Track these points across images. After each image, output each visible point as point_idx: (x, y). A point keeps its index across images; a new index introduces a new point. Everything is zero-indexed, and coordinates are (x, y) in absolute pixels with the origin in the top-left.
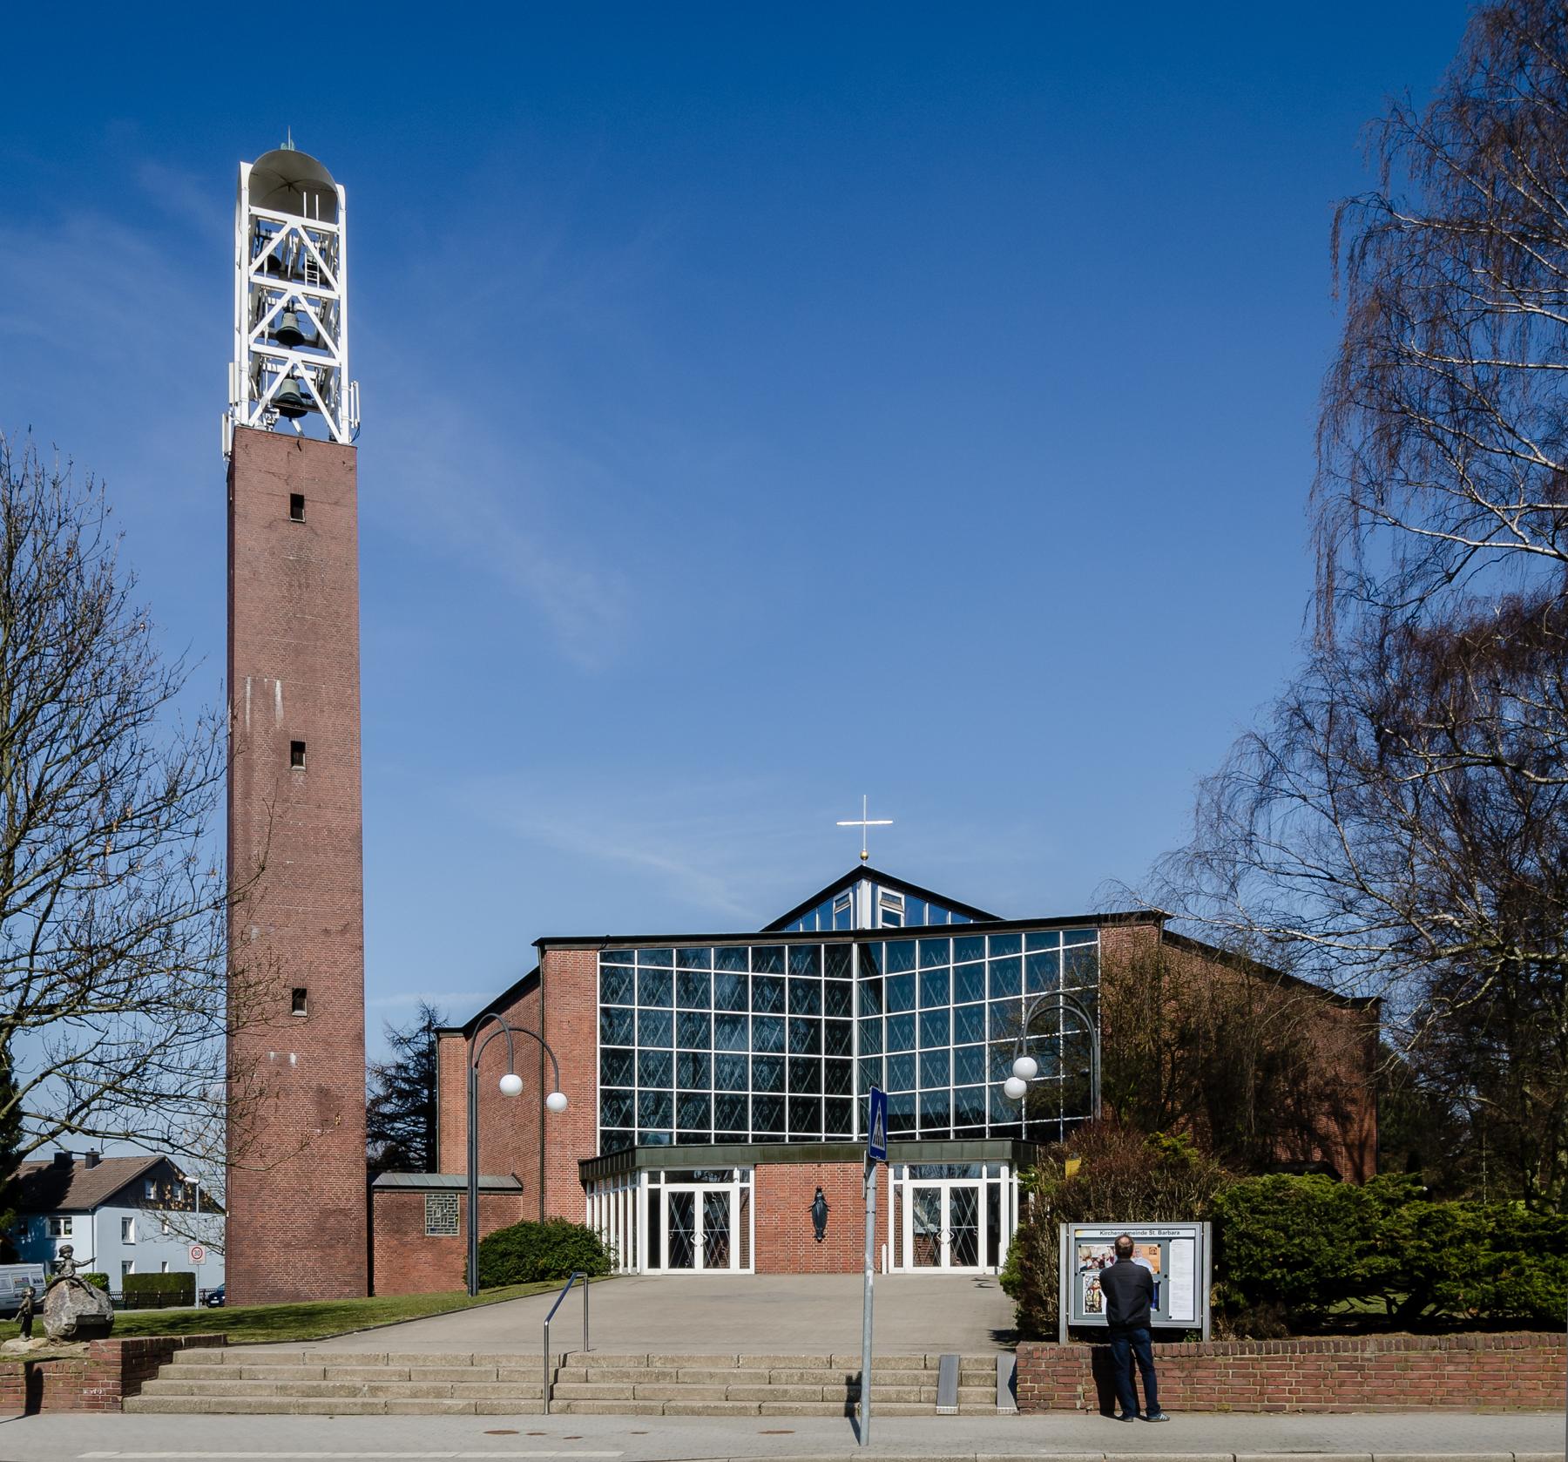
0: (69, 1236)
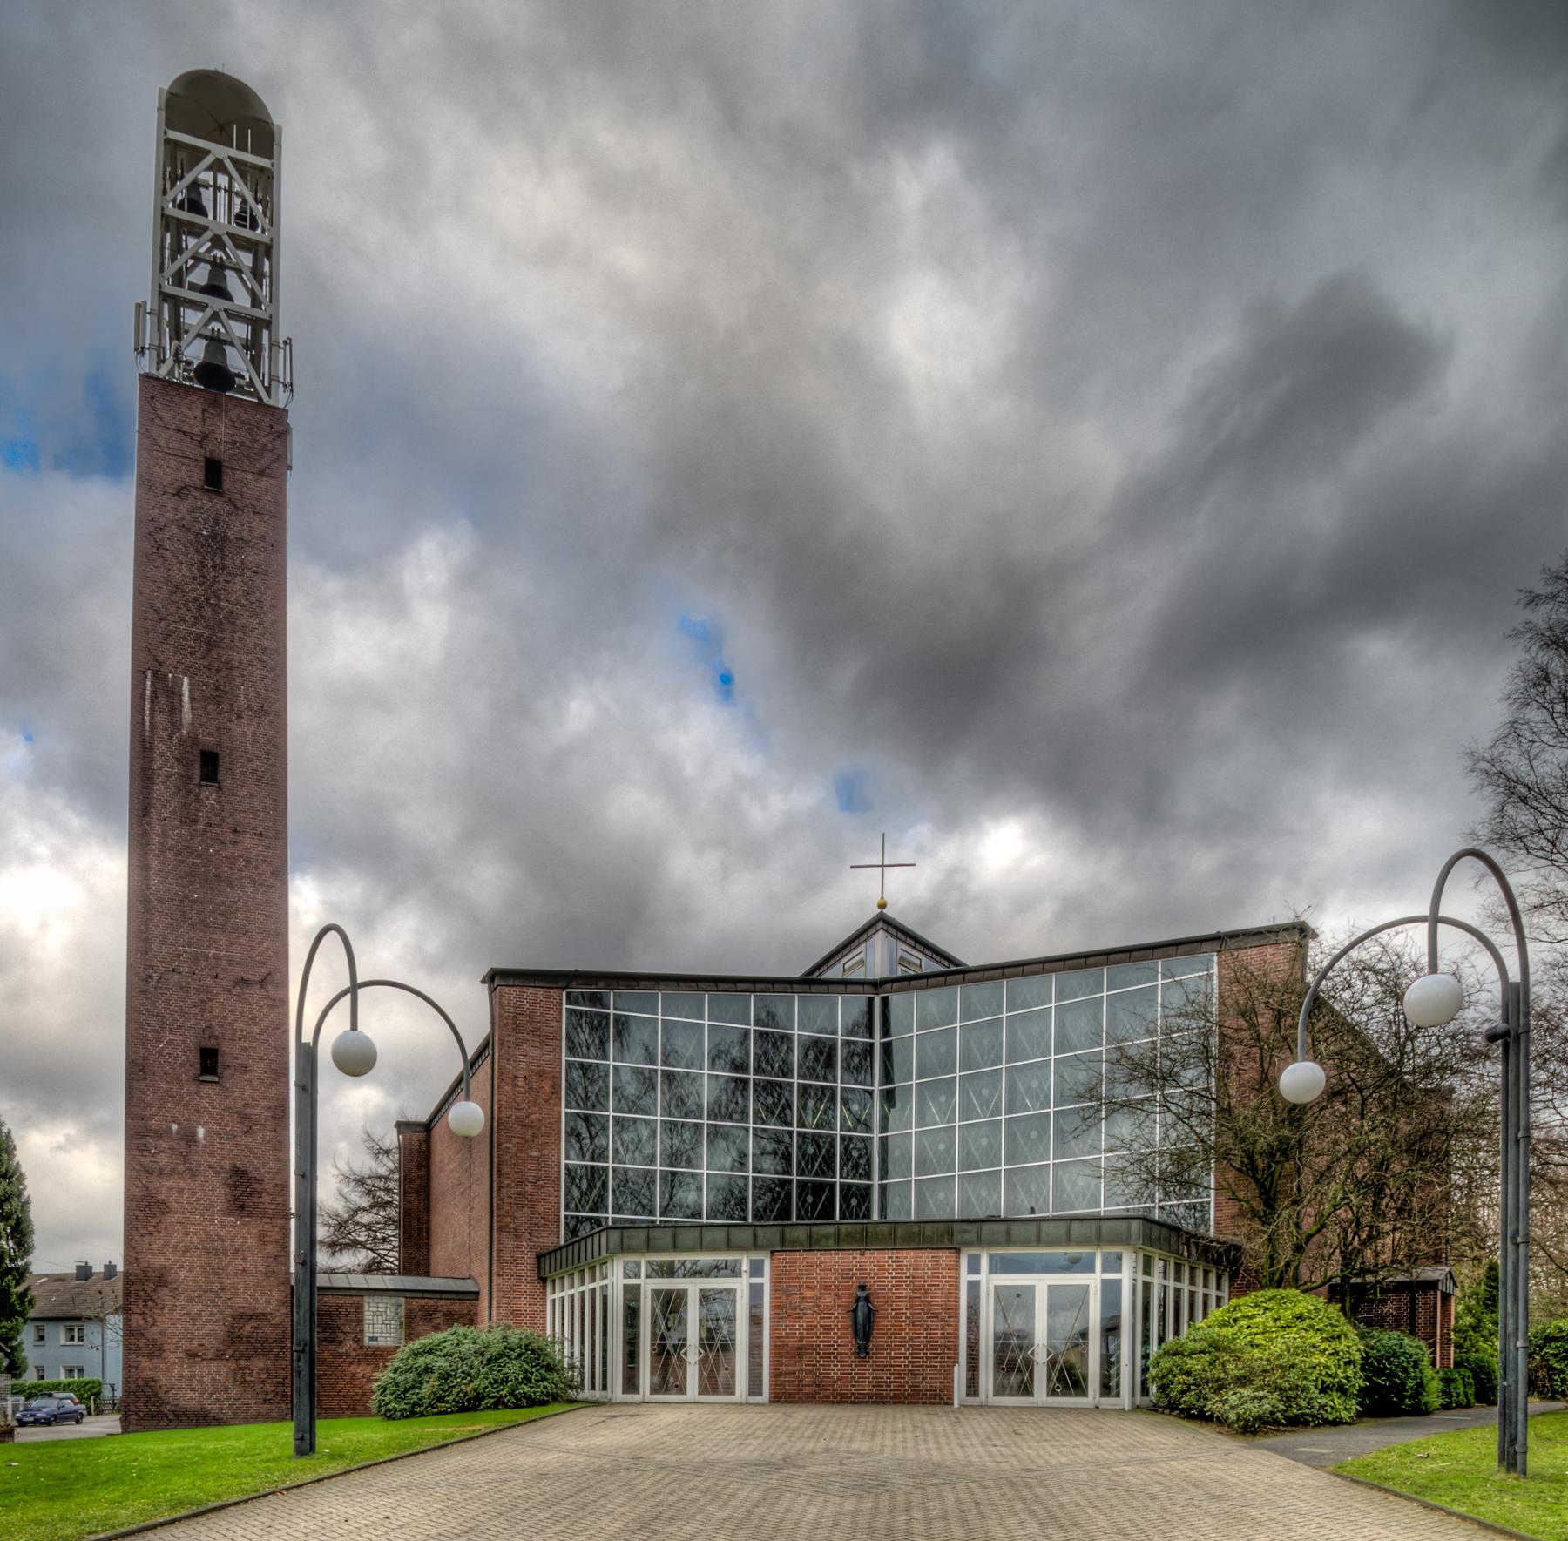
0: (81, 1343)
